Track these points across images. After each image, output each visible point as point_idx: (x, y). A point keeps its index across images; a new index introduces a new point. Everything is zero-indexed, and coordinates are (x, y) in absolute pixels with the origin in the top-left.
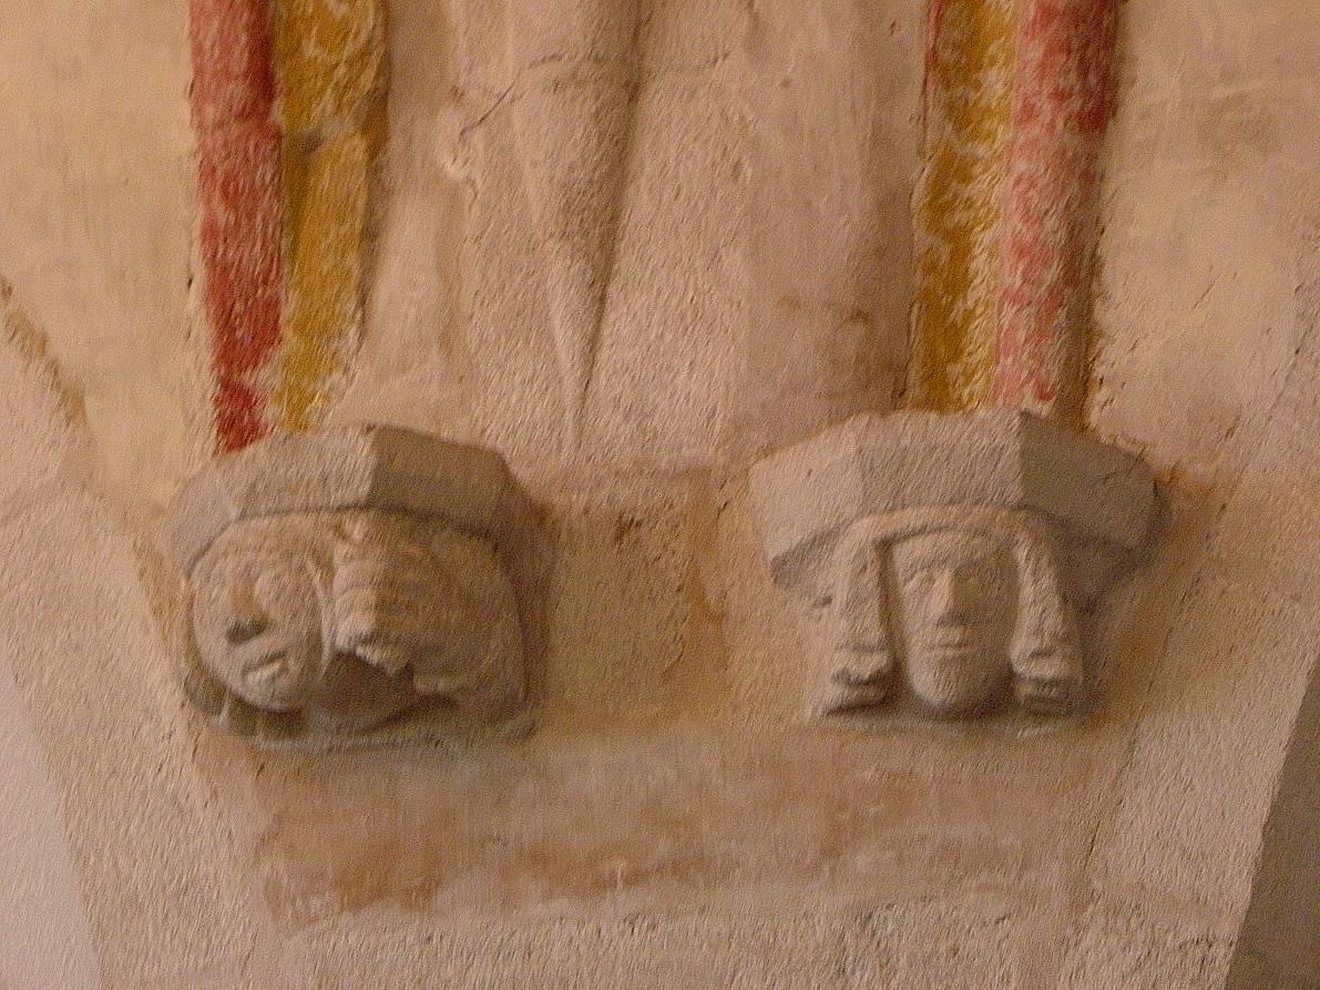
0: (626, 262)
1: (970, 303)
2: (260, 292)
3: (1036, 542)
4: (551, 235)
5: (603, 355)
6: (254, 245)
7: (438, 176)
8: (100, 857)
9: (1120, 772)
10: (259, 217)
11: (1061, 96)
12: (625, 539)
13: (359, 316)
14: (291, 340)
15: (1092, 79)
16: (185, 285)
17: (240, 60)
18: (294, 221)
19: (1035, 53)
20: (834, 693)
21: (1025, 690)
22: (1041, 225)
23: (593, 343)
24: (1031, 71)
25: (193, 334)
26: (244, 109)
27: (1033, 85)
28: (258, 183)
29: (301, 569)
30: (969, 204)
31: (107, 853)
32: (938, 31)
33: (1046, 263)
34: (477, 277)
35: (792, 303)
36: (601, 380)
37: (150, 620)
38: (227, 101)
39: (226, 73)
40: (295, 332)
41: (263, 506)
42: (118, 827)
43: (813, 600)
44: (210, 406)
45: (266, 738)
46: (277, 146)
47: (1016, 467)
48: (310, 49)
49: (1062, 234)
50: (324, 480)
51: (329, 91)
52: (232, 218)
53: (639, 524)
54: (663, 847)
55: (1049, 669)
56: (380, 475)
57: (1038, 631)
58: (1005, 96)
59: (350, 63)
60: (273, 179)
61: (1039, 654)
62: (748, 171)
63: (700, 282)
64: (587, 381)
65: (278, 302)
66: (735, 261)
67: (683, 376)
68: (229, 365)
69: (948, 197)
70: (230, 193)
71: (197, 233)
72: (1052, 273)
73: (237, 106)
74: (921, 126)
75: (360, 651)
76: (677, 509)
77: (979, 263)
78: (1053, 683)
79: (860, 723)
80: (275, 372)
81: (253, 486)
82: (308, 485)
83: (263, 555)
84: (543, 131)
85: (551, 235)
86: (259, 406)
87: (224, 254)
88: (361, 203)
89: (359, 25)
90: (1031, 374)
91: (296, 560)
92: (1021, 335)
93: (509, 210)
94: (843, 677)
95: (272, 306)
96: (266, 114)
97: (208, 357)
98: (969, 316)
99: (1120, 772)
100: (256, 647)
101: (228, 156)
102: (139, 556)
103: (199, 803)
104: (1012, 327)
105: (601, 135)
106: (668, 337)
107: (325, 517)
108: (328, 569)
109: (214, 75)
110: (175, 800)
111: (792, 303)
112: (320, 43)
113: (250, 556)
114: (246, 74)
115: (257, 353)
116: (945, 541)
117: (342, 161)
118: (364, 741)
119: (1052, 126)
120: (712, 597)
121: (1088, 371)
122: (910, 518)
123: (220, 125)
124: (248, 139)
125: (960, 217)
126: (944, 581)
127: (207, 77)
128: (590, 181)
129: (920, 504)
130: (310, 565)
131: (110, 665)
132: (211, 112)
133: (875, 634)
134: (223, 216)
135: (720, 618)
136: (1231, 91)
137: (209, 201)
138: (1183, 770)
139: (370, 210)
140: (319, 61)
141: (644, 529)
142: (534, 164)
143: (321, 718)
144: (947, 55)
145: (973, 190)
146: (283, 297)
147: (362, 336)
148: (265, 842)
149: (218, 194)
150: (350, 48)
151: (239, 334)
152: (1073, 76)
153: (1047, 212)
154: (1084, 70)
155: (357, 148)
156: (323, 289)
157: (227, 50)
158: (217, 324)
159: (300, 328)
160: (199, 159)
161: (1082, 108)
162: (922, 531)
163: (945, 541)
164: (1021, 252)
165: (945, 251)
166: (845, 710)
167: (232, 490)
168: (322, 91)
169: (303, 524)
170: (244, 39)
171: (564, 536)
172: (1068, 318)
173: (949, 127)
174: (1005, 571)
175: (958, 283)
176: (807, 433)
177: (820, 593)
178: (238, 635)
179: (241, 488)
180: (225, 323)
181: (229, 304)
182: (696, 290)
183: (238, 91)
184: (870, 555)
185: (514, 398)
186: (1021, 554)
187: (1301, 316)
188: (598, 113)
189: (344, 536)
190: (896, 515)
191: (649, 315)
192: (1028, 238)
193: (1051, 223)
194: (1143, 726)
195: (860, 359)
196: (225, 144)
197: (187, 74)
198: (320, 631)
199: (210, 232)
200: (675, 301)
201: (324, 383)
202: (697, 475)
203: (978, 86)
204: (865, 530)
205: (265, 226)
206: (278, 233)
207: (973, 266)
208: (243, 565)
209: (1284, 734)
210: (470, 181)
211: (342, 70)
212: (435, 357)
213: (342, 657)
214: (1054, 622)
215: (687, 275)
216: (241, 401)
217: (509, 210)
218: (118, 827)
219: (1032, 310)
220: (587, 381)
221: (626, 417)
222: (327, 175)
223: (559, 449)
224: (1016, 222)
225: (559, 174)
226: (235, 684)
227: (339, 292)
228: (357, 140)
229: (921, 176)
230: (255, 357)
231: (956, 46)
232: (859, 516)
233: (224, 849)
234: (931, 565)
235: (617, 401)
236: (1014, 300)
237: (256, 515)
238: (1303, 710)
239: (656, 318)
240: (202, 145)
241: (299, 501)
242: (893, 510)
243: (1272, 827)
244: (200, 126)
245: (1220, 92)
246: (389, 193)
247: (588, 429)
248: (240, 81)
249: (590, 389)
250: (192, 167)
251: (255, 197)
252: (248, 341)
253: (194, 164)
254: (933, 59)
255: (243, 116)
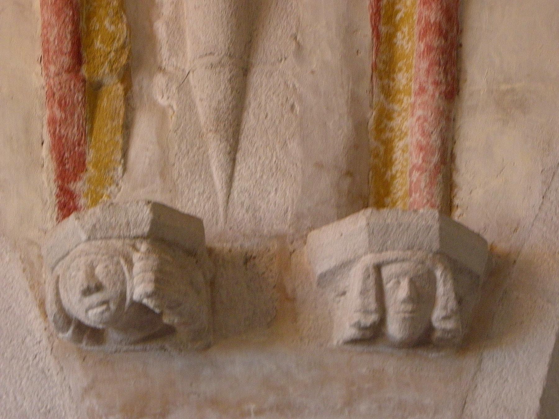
0: (244, 144)
1: (394, 172)
2: (76, 148)
3: (445, 268)
4: (210, 131)
5: (236, 184)
6: (74, 127)
7: (155, 104)
8: (8, 396)
9: (475, 374)
10: (76, 116)
11: (437, 84)
12: (248, 264)
13: (122, 161)
14: (91, 170)
15: (449, 78)
16: (40, 144)
17: (67, 46)
18: (91, 118)
19: (424, 65)
20: (350, 332)
21: (438, 334)
22: (430, 137)
23: (231, 178)
24: (422, 73)
25: (45, 166)
26: (69, 68)
27: (423, 78)
28: (75, 101)
29: (118, 263)
30: (392, 130)
31: (11, 394)
32: (377, 55)
33: (433, 154)
34: (176, 148)
35: (319, 166)
36: (235, 194)
37: (29, 291)
38: (61, 63)
39: (61, 51)
40: (93, 166)
41: (99, 234)
42: (16, 382)
43: (336, 293)
44: (54, 197)
45: (86, 344)
46: (84, 86)
47: (438, 234)
48: (98, 44)
49: (439, 142)
50: (128, 224)
51: (106, 63)
52: (63, 116)
53: (255, 258)
54: (272, 399)
55: (449, 325)
56: (154, 224)
57: (445, 308)
58: (407, 84)
59: (116, 51)
60: (82, 99)
61: (446, 318)
62: (297, 108)
63: (278, 154)
64: (229, 195)
65: (85, 153)
66: (294, 146)
67: (273, 194)
68: (63, 180)
69: (383, 126)
70: (62, 105)
71: (45, 122)
72: (436, 158)
73: (66, 66)
74: (371, 94)
75: (145, 301)
76: (271, 253)
77: (398, 154)
78: (449, 331)
79: (358, 348)
80: (84, 184)
81: (94, 226)
82: (120, 226)
83: (99, 256)
84: (206, 85)
85: (210, 131)
86: (77, 198)
87: (60, 131)
88: (122, 113)
89: (120, 36)
90: (428, 201)
91: (115, 259)
92: (423, 185)
93: (190, 119)
94: (358, 325)
95: (82, 155)
96: (79, 71)
97: (53, 176)
98: (393, 177)
99: (475, 374)
100: (96, 298)
101: (61, 88)
102: (23, 262)
103: (55, 373)
104: (418, 181)
105: (232, 89)
106: (265, 177)
107: (127, 241)
108: (130, 263)
109: (55, 52)
110: (43, 372)
111: (319, 166)
112: (103, 42)
113: (93, 257)
114: (70, 53)
115: (76, 175)
116: (406, 266)
117: (112, 94)
118: (132, 347)
119: (433, 96)
120: (289, 291)
121: (451, 201)
122: (389, 255)
123: (58, 74)
124: (70, 81)
125: (388, 134)
126: (405, 284)
127: (51, 54)
128: (228, 108)
129: (394, 249)
130: (122, 262)
131: (10, 310)
132: (52, 68)
133: (373, 306)
134: (59, 114)
135: (293, 300)
136: (509, 87)
137: (52, 107)
138: (503, 374)
139: (126, 116)
140: (102, 49)
141: (257, 261)
142: (201, 100)
143: (113, 335)
144: (381, 66)
145: (393, 124)
146: (87, 152)
147: (125, 170)
148: (86, 391)
149: (56, 105)
150: (116, 45)
151: (67, 166)
152: (442, 75)
153: (432, 133)
154: (446, 72)
155: (119, 88)
156: (105, 148)
157: (61, 41)
158: (57, 162)
159: (96, 166)
160: (46, 89)
161: (446, 89)
162: (396, 261)
163: (406, 266)
164: (421, 149)
165: (382, 149)
166: (354, 341)
167: (83, 227)
168: (103, 63)
169: (119, 244)
170: (69, 37)
171: (220, 262)
172: (443, 178)
173: (382, 97)
174: (432, 281)
175: (388, 163)
176: (327, 221)
177: (341, 289)
178: (87, 292)
179: (88, 226)
180: (61, 161)
181: (62, 153)
182: (277, 158)
183: (66, 60)
184: (371, 271)
185: (195, 201)
186: (438, 273)
187: (544, 182)
188: (230, 79)
189: (137, 250)
190: (383, 254)
191: (256, 168)
192: (424, 143)
193: (434, 137)
194: (485, 354)
195: (349, 192)
196: (60, 83)
197: (39, 53)
198: (126, 292)
199: (52, 121)
200: (267, 162)
201: (107, 190)
202: (280, 237)
203: (394, 80)
204: (369, 259)
205: (79, 120)
206: (84, 124)
207: (394, 156)
208: (89, 261)
209: (547, 359)
210: (171, 106)
211: (113, 54)
212: (158, 180)
213: (133, 303)
214: (452, 304)
215: (272, 151)
216: (69, 196)
217: (190, 119)
218: (16, 382)
219: (427, 174)
220: (229, 195)
221: (247, 211)
222: (105, 99)
223: (217, 223)
224: (418, 136)
225: (214, 104)
226: (82, 317)
227: (113, 150)
228: (119, 85)
229: (371, 116)
230: (76, 177)
231: (384, 62)
232: (365, 254)
233: (67, 394)
234: (398, 277)
235: (242, 204)
236: (418, 169)
237: (95, 239)
238: (555, 349)
239: (259, 169)
240: (48, 84)
241: (116, 233)
242: (382, 251)
243: (543, 400)
244: (47, 75)
245: (503, 87)
246: (133, 109)
247: (229, 216)
248: (67, 55)
249: (230, 197)
250: (43, 93)
251: (74, 106)
252: (71, 170)
253: (43, 93)
254: (375, 67)
255: (68, 71)
